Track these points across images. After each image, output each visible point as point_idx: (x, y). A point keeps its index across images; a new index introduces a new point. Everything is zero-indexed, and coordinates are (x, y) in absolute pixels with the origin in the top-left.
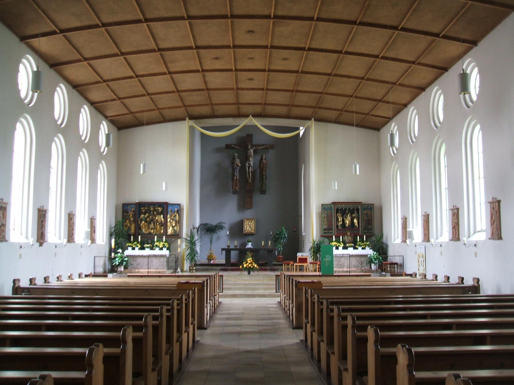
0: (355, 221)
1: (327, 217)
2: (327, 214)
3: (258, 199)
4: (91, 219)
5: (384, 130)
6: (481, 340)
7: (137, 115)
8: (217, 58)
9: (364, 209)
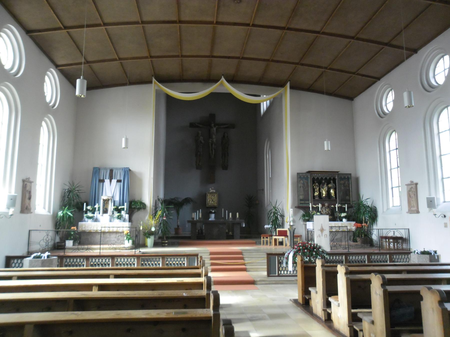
0: (332, 191)
1: (303, 187)
2: (304, 184)
3: (220, 174)
4: (24, 181)
5: (360, 100)
7: (95, 66)
9: (341, 179)
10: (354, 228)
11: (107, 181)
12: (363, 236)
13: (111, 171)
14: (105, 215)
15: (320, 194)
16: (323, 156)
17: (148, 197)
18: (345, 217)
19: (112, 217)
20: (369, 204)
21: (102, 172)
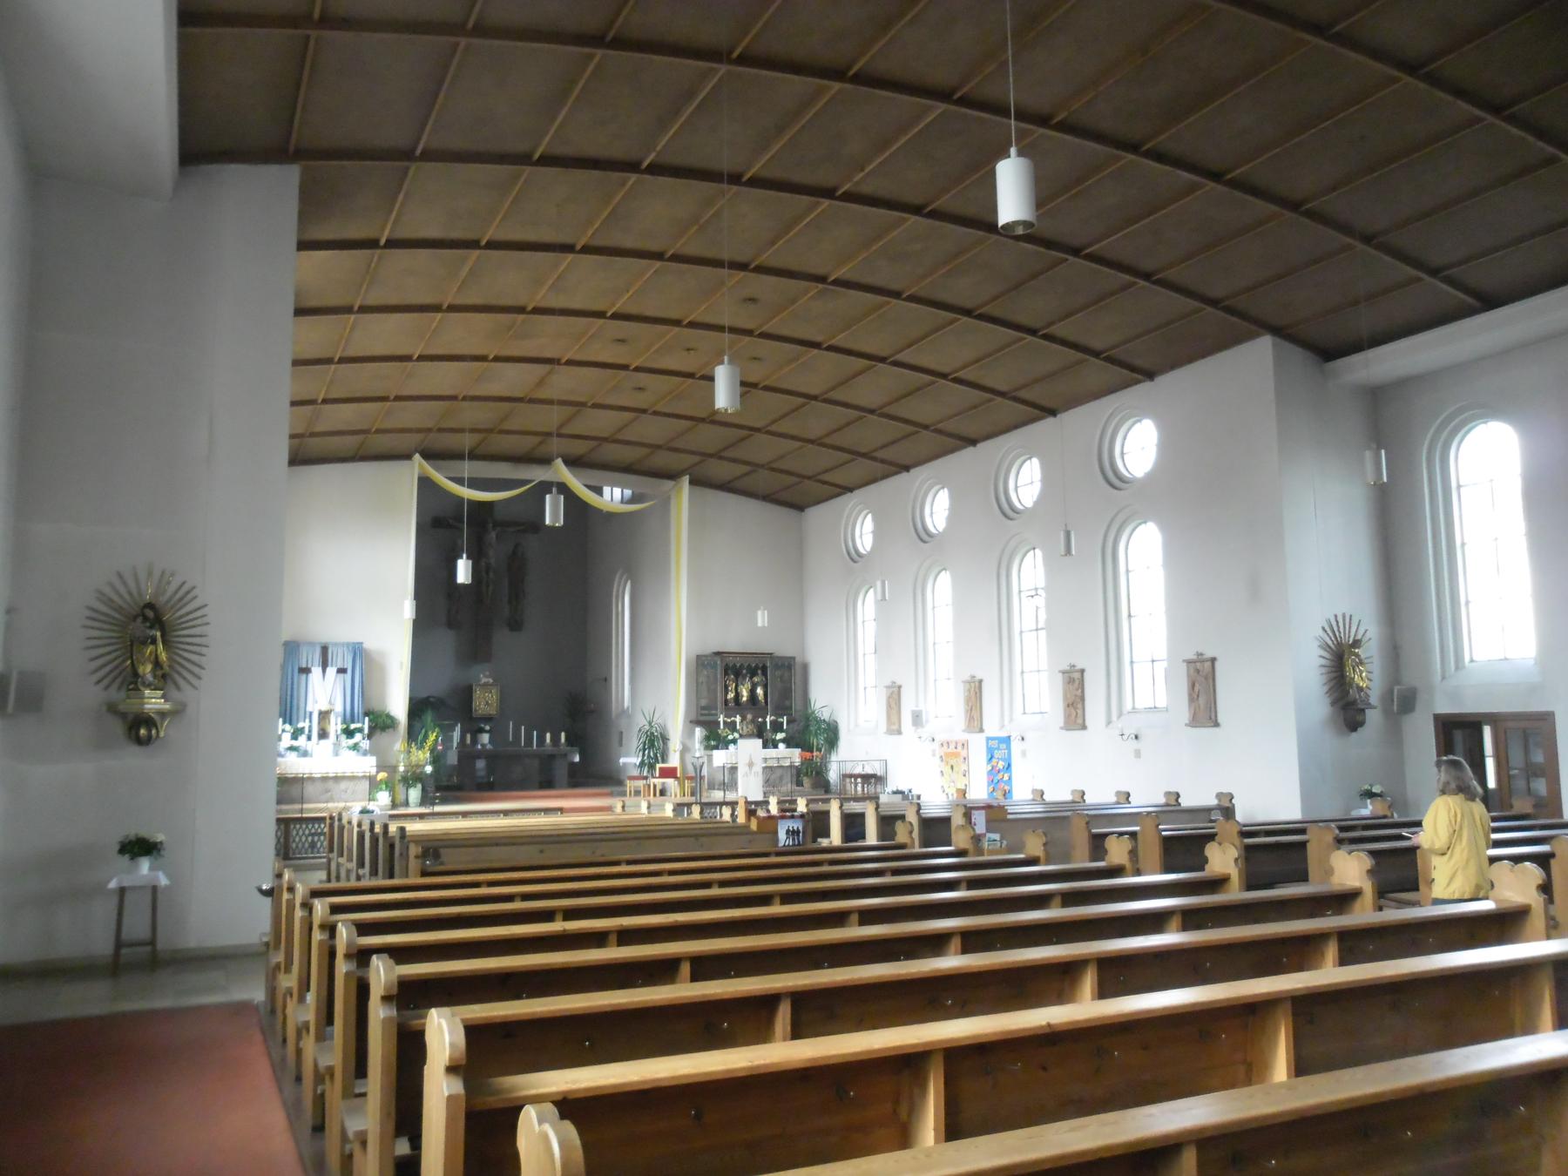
0: (759, 691)
3: (502, 639)
5: (817, 516)
6: (1154, 922)
8: (622, 341)
10: (797, 761)
11: (316, 671)
12: (813, 775)
13: (325, 650)
14: (323, 742)
15: (738, 695)
16: (753, 628)
17: (398, 704)
18: (783, 741)
19: (337, 745)
20: (825, 715)
21: (304, 652)
